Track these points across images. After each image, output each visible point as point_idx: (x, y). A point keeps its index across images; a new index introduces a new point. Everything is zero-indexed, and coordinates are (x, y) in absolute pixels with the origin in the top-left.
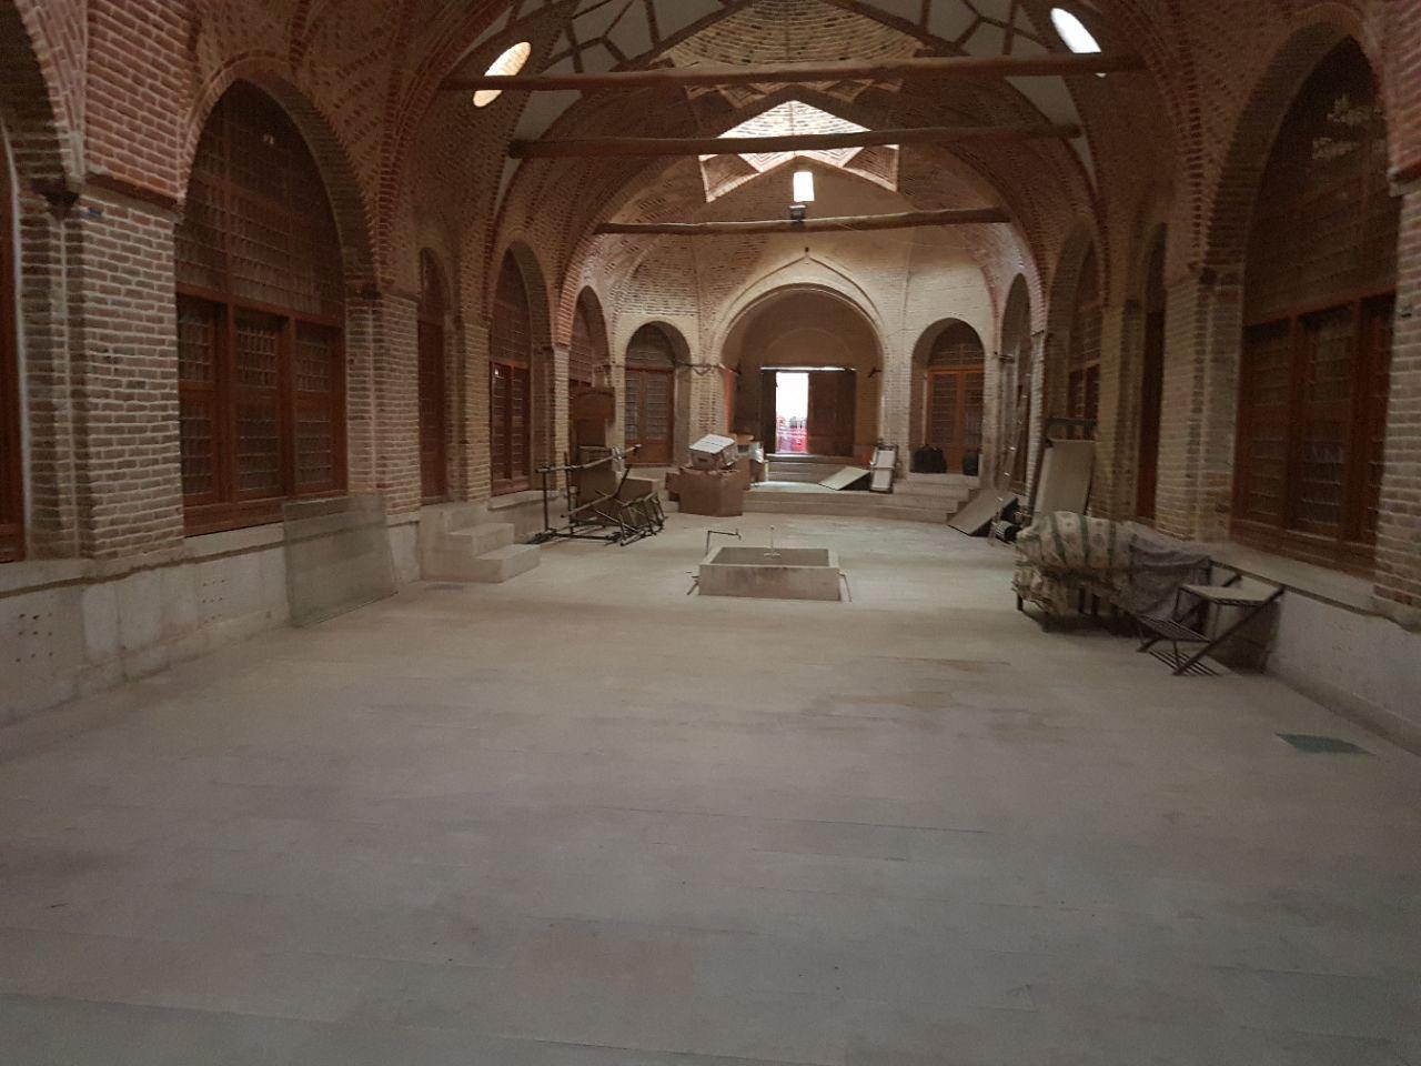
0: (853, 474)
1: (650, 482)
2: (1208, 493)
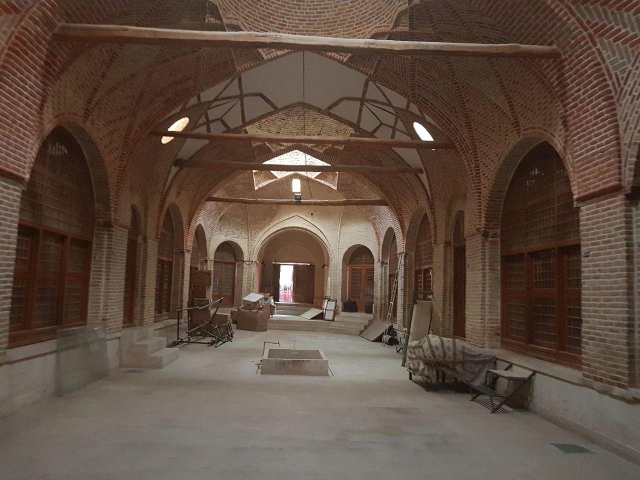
0: (314, 312)
1: (227, 316)
2: (491, 327)
